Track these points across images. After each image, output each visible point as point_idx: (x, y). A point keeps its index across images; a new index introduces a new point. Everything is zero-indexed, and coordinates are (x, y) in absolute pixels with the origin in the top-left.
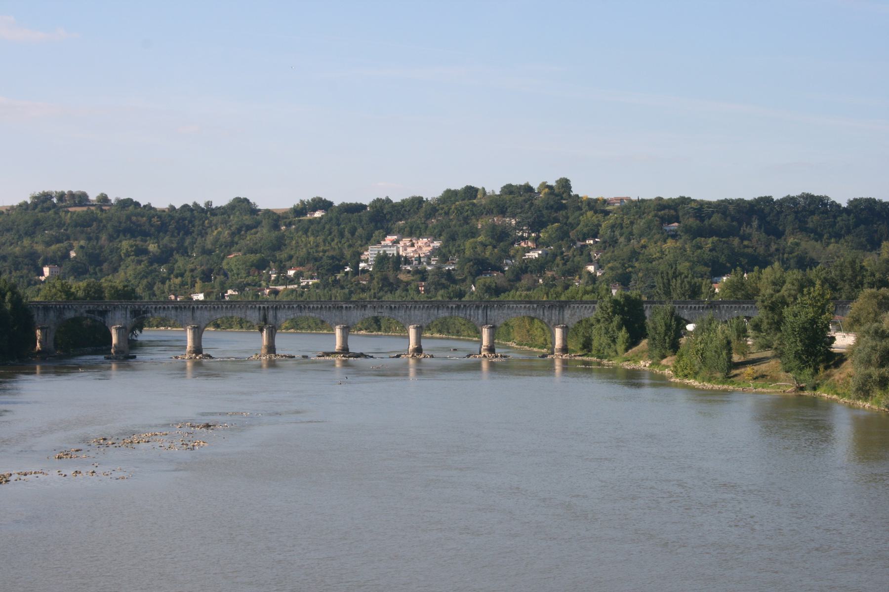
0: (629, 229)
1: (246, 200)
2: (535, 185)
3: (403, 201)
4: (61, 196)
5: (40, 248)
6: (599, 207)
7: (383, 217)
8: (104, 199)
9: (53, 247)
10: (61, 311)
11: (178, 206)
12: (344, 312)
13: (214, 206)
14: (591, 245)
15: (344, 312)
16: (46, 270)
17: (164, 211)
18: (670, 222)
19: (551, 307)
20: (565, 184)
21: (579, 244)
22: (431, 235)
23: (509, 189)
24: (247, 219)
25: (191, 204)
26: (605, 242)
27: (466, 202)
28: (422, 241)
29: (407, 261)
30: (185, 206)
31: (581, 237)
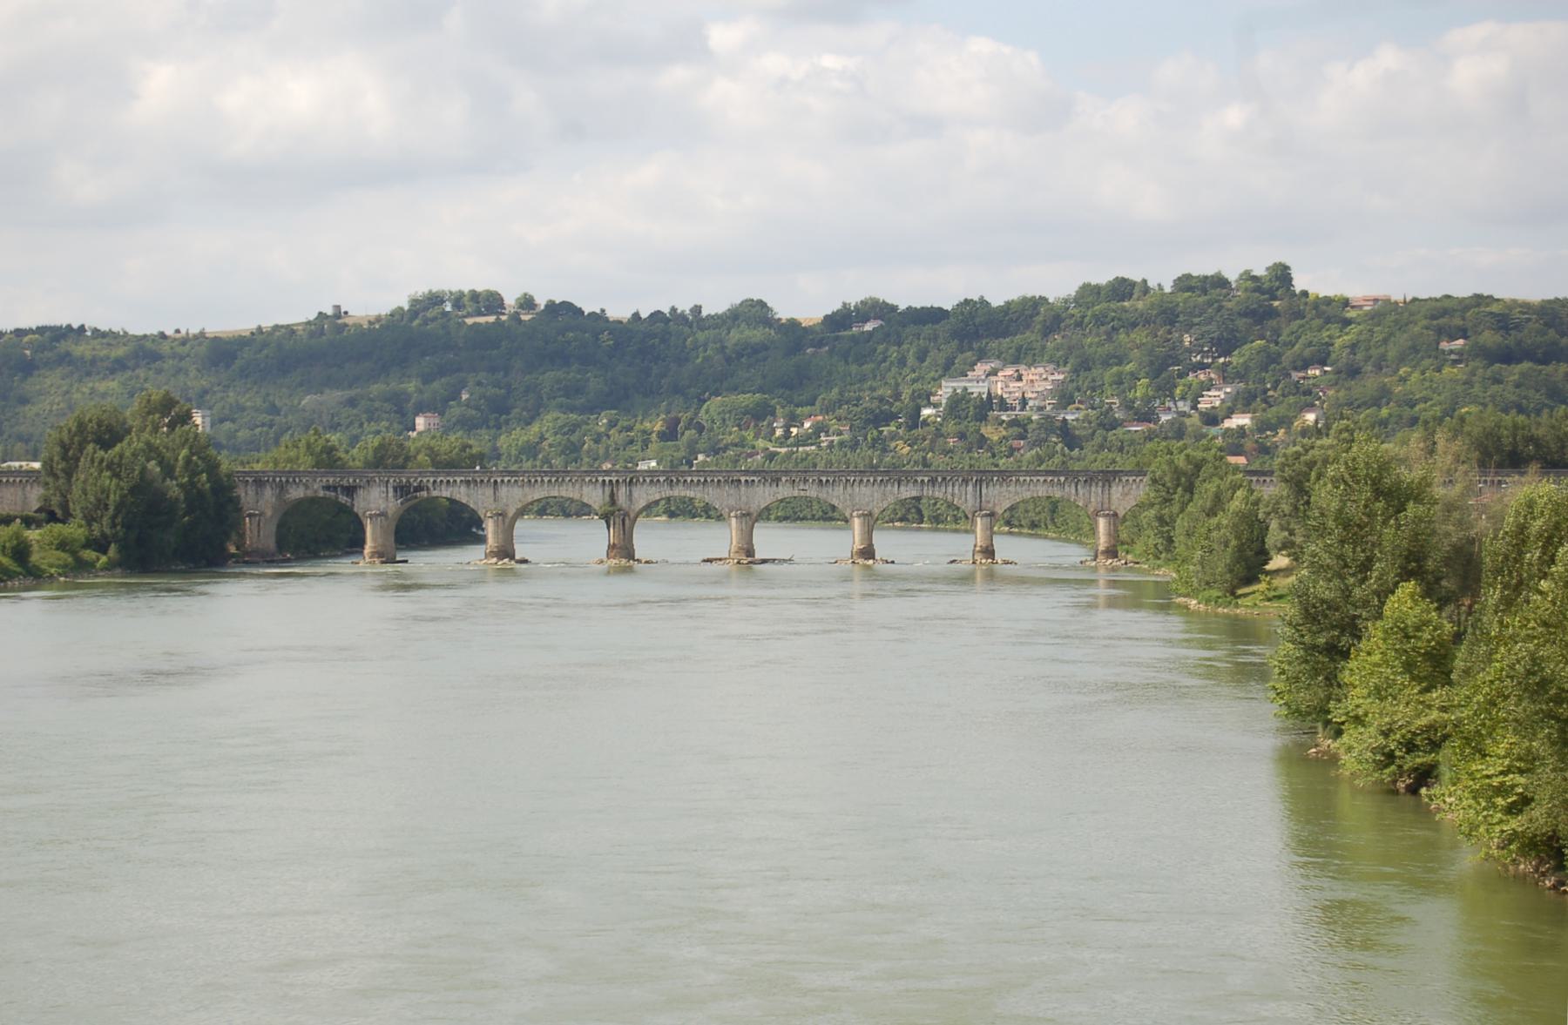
0: (1382, 350)
1: (762, 304)
2: (1232, 276)
3: (1008, 303)
4: (458, 300)
5: (411, 386)
6: (1329, 310)
7: (979, 329)
8: (527, 303)
9: (436, 385)
10: (282, 488)
11: (644, 315)
12: (743, 489)
13: (704, 313)
14: (1315, 377)
15: (743, 489)
16: (420, 422)
17: (620, 322)
18: (1452, 338)
19: (1090, 480)
20: (1282, 274)
21: (1296, 375)
22: (1050, 361)
23: (1186, 283)
24: (757, 335)
25: (666, 310)
26: (1339, 372)
27: (1113, 305)
28: (1030, 374)
29: (1004, 406)
30: (657, 316)
31: (1299, 363)
